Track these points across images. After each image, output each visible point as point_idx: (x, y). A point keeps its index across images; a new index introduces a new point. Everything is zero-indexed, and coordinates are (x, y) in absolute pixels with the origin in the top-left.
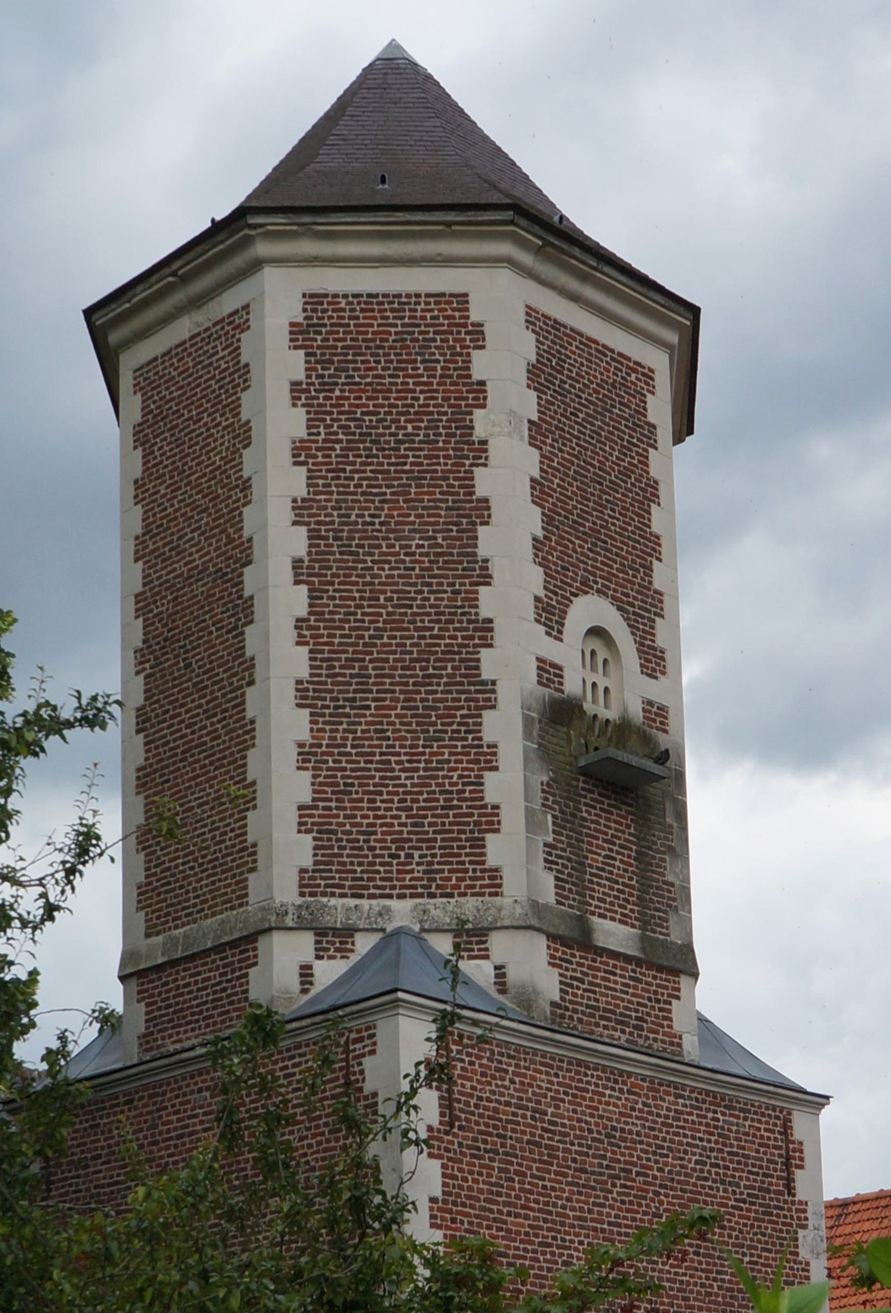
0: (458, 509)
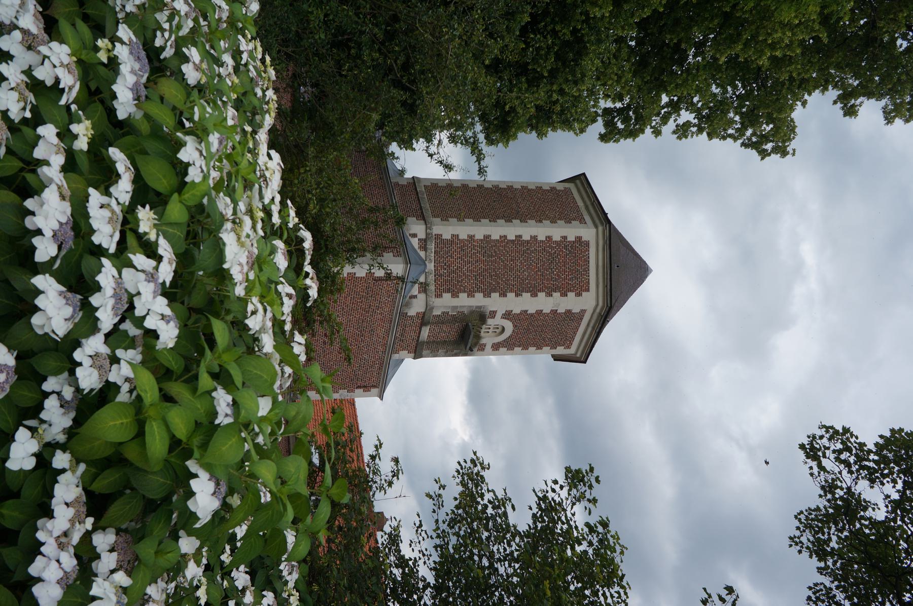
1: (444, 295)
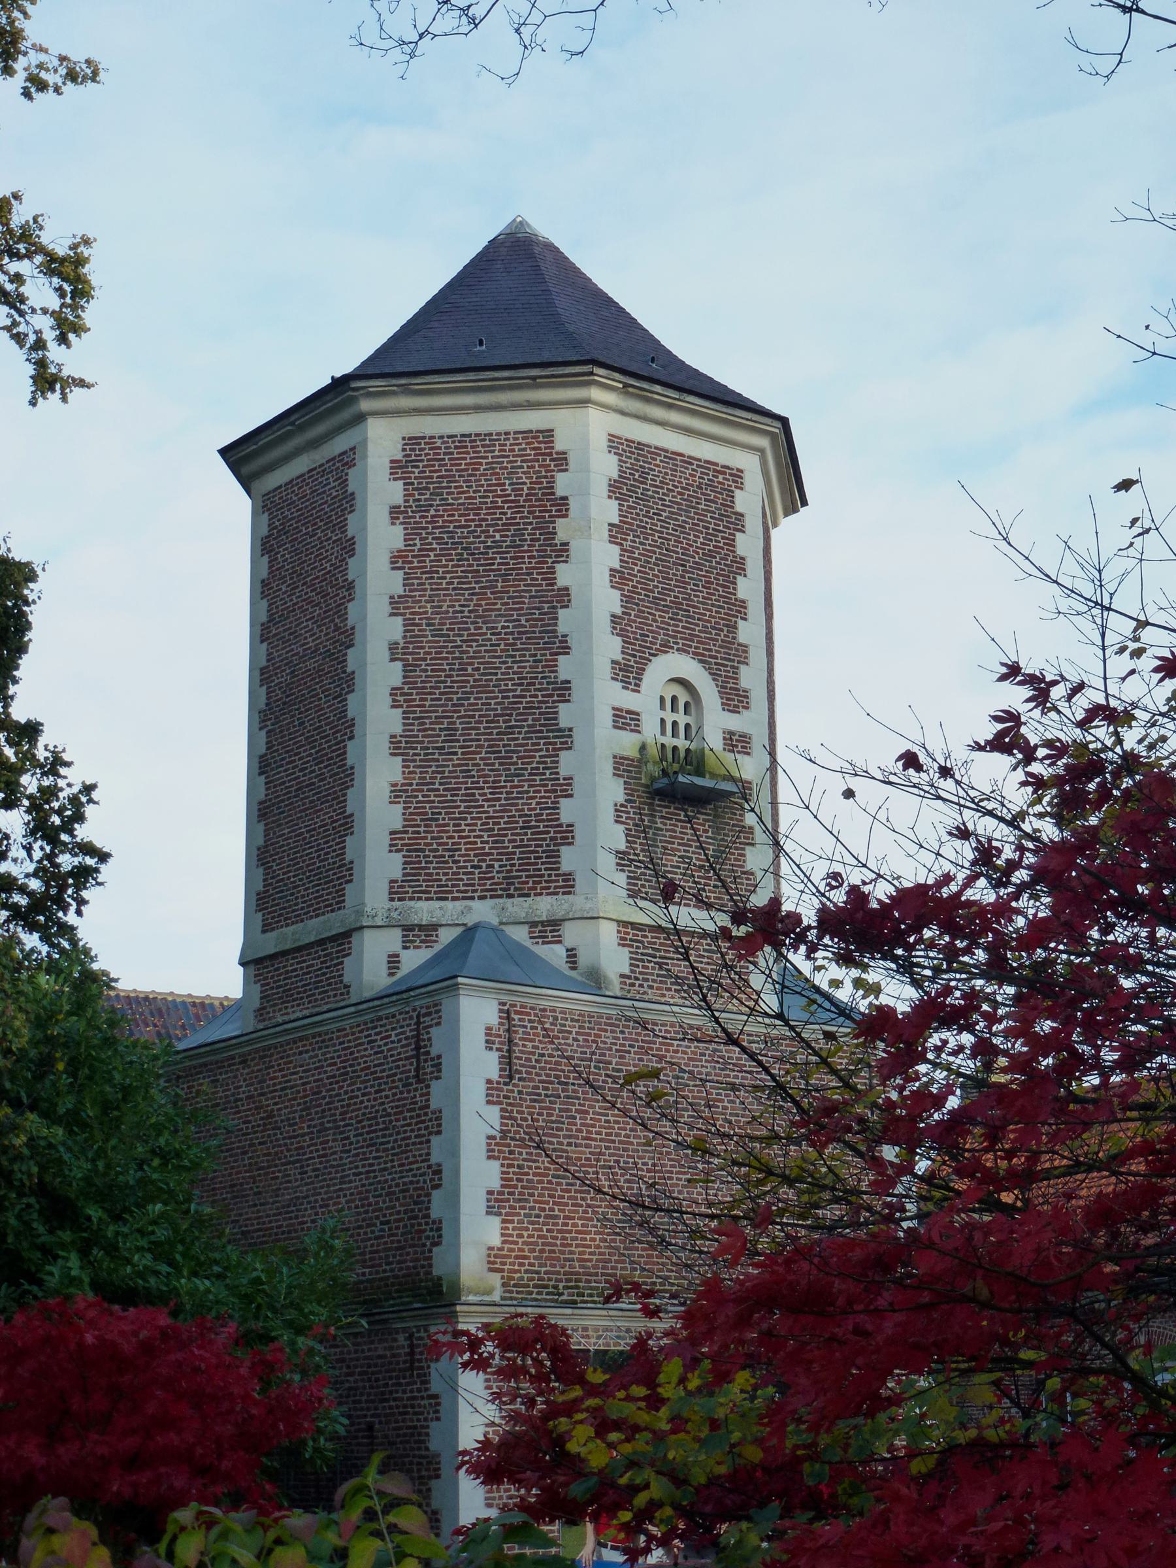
0: (542, 596)
1: (565, 867)
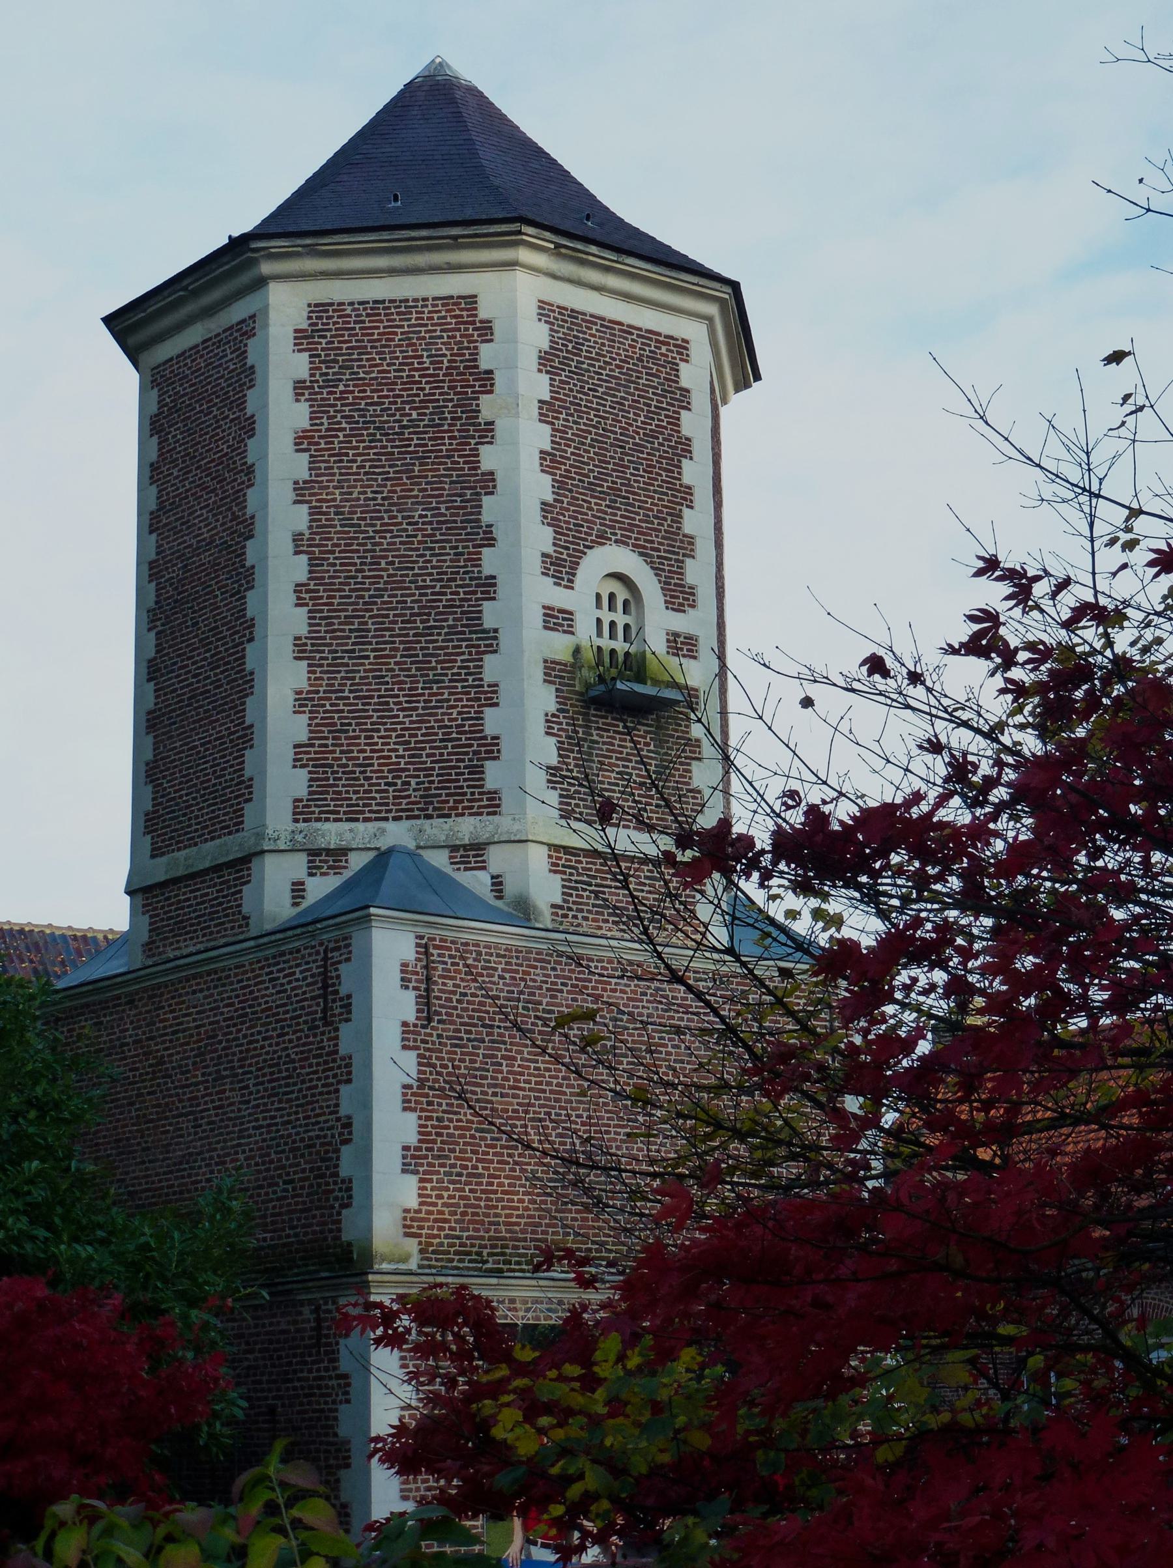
1: (490, 785)
